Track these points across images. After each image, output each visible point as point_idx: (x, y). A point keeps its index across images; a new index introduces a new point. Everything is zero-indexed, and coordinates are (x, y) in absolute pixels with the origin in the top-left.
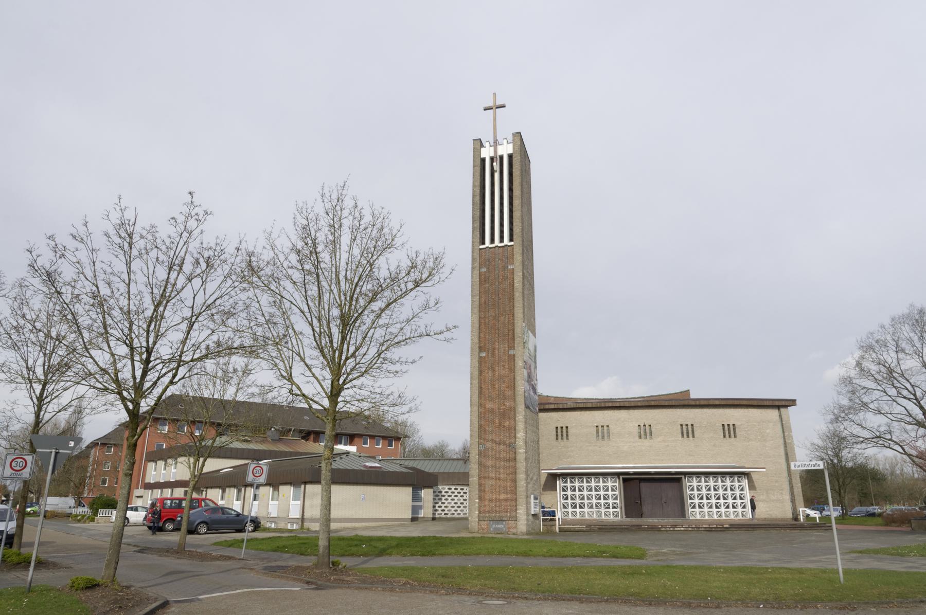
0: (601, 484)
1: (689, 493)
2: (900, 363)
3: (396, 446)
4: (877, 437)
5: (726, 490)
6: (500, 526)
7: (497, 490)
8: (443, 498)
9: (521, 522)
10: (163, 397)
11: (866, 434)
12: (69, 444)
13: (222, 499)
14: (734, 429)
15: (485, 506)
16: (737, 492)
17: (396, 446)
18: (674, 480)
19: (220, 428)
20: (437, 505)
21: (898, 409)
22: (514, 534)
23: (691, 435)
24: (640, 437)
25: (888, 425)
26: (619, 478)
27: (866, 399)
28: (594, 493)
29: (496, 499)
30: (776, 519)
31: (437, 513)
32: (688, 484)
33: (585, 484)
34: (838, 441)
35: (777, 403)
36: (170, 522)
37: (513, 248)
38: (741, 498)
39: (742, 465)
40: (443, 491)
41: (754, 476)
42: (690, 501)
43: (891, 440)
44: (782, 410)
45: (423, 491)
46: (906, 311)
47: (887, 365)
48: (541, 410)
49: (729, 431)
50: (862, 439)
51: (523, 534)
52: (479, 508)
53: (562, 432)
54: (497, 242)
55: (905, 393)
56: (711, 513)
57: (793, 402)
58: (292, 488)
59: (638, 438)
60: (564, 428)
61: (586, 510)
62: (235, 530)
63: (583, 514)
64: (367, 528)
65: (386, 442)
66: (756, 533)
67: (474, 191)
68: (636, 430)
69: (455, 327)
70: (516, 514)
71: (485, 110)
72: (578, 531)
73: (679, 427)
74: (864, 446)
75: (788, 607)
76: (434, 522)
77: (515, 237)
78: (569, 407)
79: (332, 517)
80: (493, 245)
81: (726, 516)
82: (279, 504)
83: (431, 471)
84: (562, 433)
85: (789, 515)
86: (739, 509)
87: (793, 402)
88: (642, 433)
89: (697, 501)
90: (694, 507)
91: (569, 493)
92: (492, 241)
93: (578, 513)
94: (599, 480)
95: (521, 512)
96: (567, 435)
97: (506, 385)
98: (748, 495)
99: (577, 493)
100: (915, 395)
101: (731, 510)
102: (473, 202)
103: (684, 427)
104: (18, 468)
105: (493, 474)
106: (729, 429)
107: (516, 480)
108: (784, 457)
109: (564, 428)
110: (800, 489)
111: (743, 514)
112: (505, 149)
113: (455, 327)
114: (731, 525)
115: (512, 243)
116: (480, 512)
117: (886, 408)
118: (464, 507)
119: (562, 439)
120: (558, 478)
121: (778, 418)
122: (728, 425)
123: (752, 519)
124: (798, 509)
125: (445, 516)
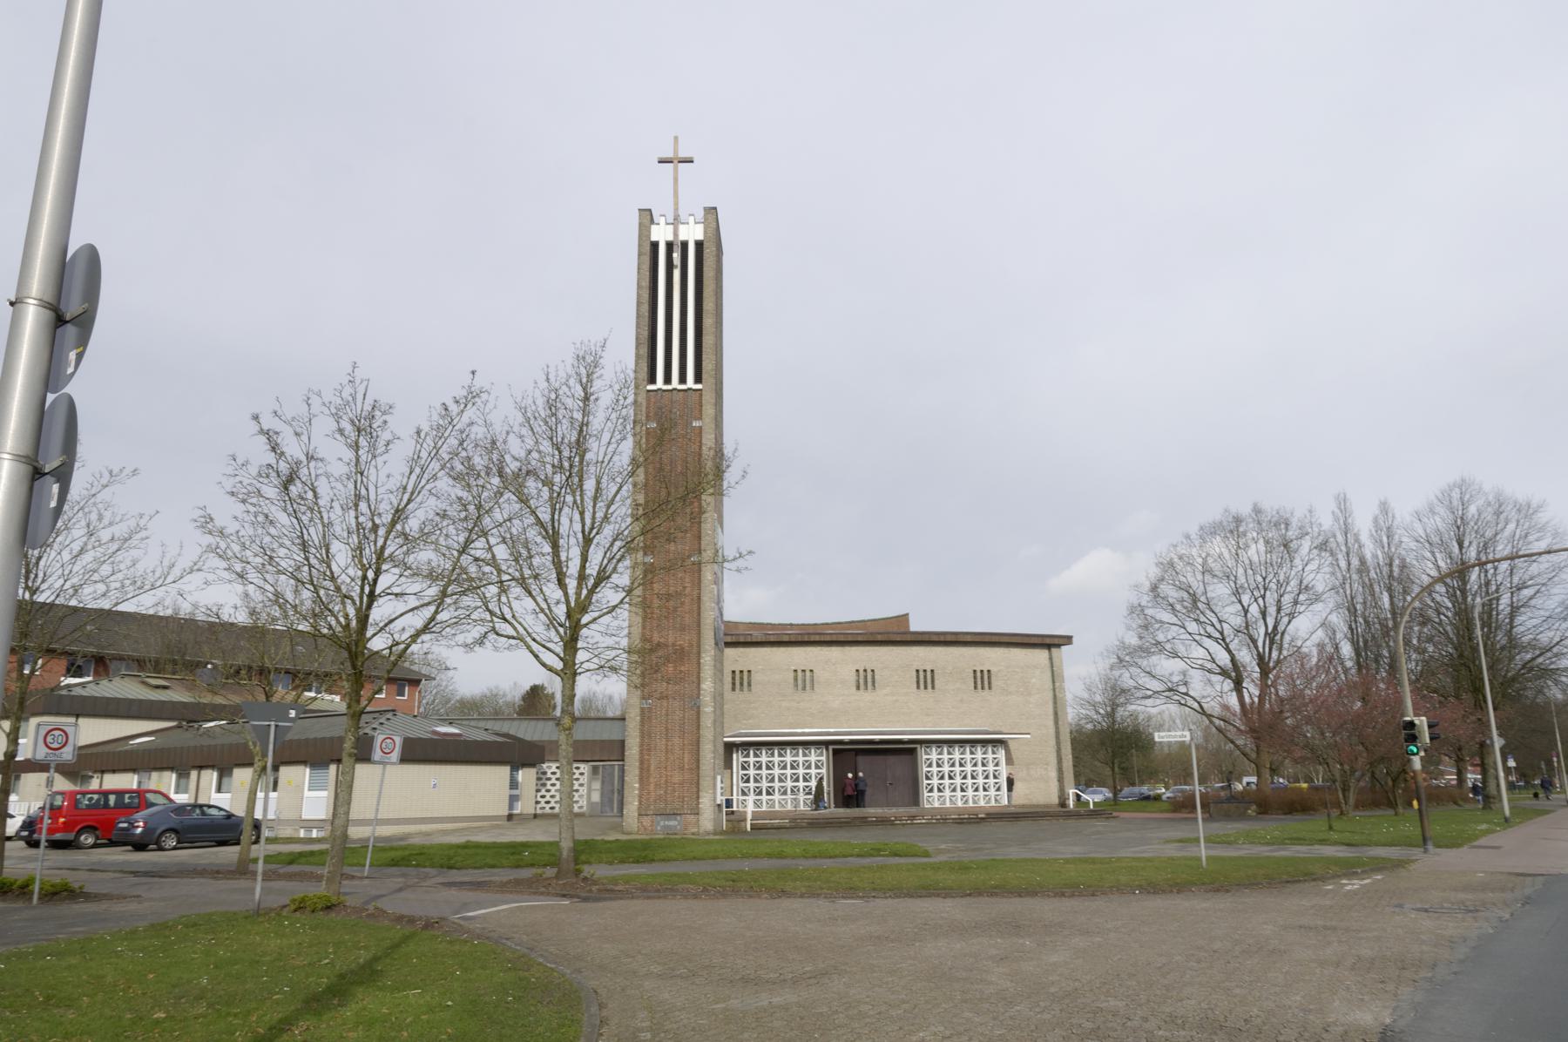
0: (801, 759)
1: (925, 769)
2: (1208, 589)
3: (411, 695)
4: (1170, 690)
5: (975, 765)
6: (673, 823)
7: (669, 768)
8: (549, 783)
9: (705, 815)
10: (562, 655)
11: (1156, 685)
12: (289, 713)
13: (219, 790)
14: (989, 678)
15: (649, 793)
16: (991, 768)
17: (411, 695)
18: (905, 751)
19: (101, 665)
20: (539, 794)
21: (1199, 653)
22: (693, 834)
23: (929, 686)
24: (858, 688)
25: (1184, 673)
26: (827, 749)
27: (1161, 637)
28: (789, 772)
29: (666, 781)
30: (1038, 806)
31: (539, 806)
32: (925, 757)
33: (776, 759)
34: (1117, 695)
35: (1048, 641)
36: (88, 832)
37: (701, 395)
38: (995, 777)
39: (997, 729)
40: (549, 772)
41: (1012, 745)
42: (926, 782)
43: (1186, 694)
44: (1054, 650)
45: (520, 772)
46: (1218, 517)
47: (1191, 592)
48: (728, 644)
49: (982, 680)
50: (1150, 693)
51: (709, 834)
52: (640, 797)
53: (742, 678)
54: (675, 383)
55: (1210, 629)
56: (953, 799)
57: (1068, 640)
58: (308, 770)
59: (855, 688)
60: (745, 674)
61: (777, 797)
62: (216, 842)
63: (771, 803)
64: (445, 832)
65: (394, 687)
66: (1023, 824)
67: (639, 296)
68: (853, 677)
69: (750, 552)
70: (698, 803)
71: (659, 162)
72: (778, 828)
73: (915, 673)
74: (1149, 702)
75: (1164, 891)
76: (537, 822)
77: (704, 376)
78: (754, 640)
79: (353, 816)
80: (669, 387)
81: (974, 802)
82: (232, 799)
83: (536, 738)
84: (741, 680)
85: (1055, 800)
86: (992, 792)
87: (1068, 640)
88: (862, 681)
89: (935, 781)
90: (931, 791)
91: (752, 772)
92: (668, 380)
93: (764, 803)
94: (798, 753)
95: (706, 803)
96: (749, 685)
97: (687, 608)
98: (1004, 771)
99: (764, 772)
100: (1222, 633)
101: (981, 793)
102: (638, 314)
103: (921, 674)
104: (55, 745)
105: (661, 744)
106: (982, 678)
107: (698, 754)
108: (1052, 717)
109: (745, 674)
110: (1071, 763)
111: (999, 798)
112: (692, 233)
113: (750, 552)
114: (987, 814)
115: (699, 386)
116: (640, 802)
117: (1182, 650)
118: (579, 796)
119: (742, 690)
120: (735, 750)
121: (1047, 662)
122: (982, 671)
123: (1008, 806)
124: (1066, 790)
125: (550, 811)
